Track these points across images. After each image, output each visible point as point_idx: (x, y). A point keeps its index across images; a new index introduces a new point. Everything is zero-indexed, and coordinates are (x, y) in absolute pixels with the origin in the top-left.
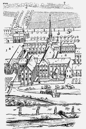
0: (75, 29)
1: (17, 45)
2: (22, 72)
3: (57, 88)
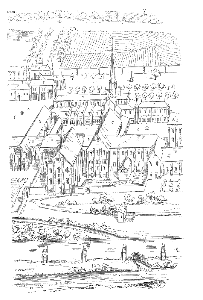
1: (38, 104)
2: (50, 166)
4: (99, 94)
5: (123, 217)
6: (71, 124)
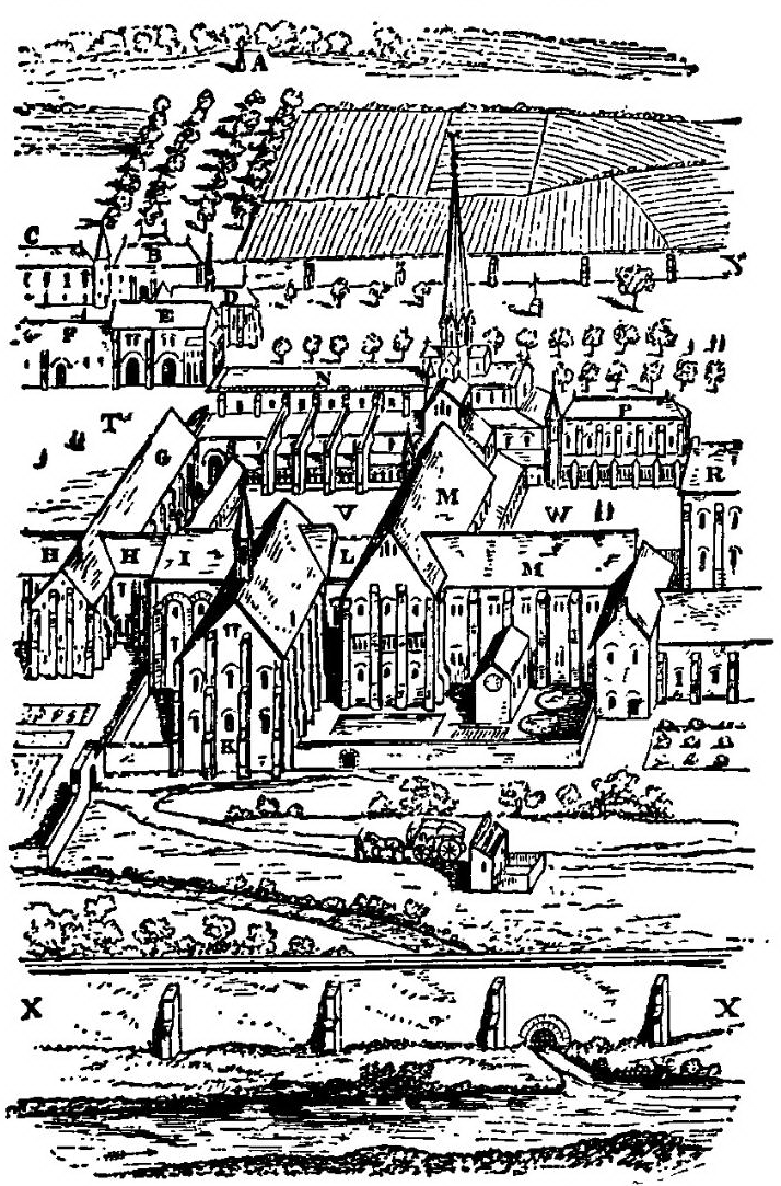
0: (685, 264)
1: (146, 404)
2: (194, 659)
3: (519, 802)
4: (308, 365)
5: (489, 867)
6: (308, 486)
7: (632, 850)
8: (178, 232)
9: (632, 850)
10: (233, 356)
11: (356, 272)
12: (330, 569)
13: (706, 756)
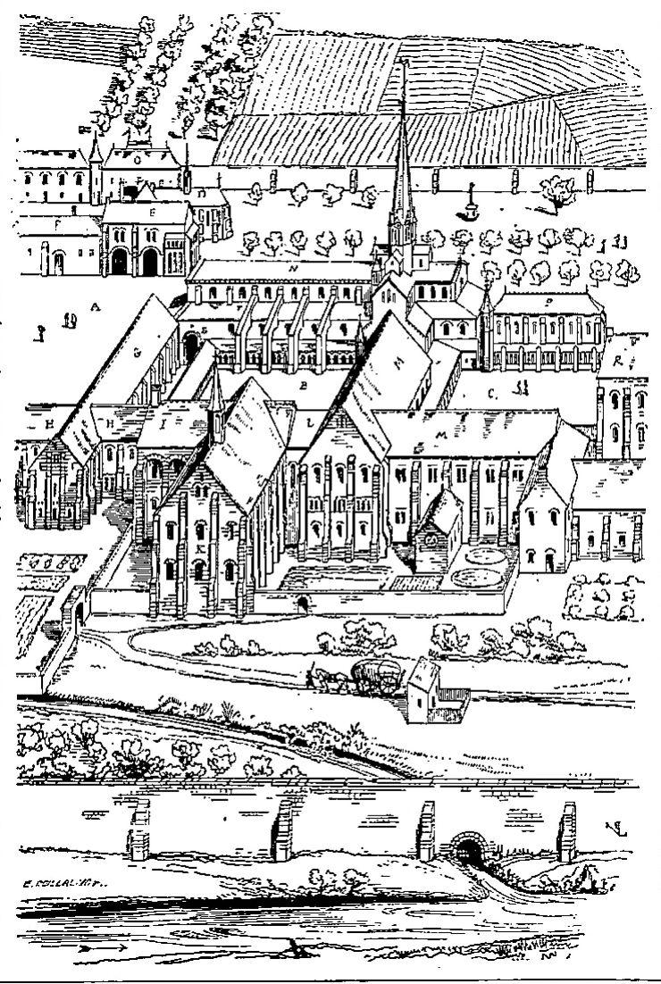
5: (424, 703)
7: (75, 59)
8: (159, 140)
9: (75, 59)
10: (206, 250)
11: (316, 179)
12: (289, 439)
13: (615, 606)
